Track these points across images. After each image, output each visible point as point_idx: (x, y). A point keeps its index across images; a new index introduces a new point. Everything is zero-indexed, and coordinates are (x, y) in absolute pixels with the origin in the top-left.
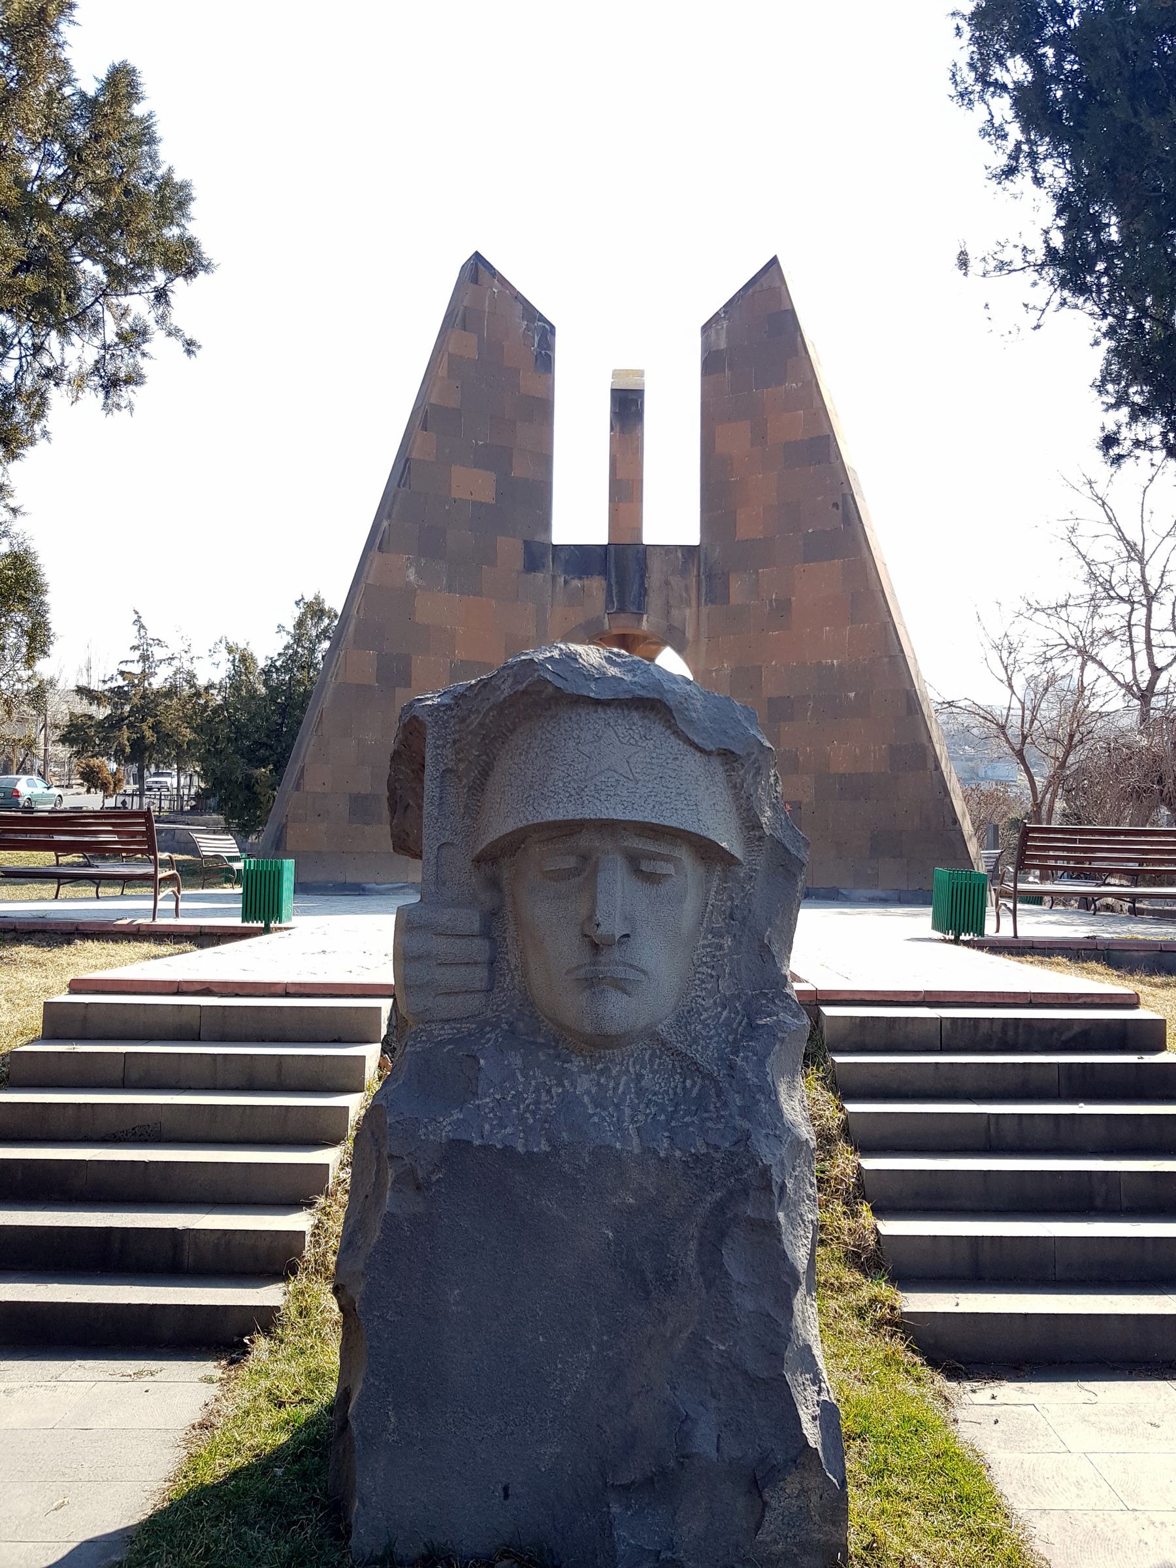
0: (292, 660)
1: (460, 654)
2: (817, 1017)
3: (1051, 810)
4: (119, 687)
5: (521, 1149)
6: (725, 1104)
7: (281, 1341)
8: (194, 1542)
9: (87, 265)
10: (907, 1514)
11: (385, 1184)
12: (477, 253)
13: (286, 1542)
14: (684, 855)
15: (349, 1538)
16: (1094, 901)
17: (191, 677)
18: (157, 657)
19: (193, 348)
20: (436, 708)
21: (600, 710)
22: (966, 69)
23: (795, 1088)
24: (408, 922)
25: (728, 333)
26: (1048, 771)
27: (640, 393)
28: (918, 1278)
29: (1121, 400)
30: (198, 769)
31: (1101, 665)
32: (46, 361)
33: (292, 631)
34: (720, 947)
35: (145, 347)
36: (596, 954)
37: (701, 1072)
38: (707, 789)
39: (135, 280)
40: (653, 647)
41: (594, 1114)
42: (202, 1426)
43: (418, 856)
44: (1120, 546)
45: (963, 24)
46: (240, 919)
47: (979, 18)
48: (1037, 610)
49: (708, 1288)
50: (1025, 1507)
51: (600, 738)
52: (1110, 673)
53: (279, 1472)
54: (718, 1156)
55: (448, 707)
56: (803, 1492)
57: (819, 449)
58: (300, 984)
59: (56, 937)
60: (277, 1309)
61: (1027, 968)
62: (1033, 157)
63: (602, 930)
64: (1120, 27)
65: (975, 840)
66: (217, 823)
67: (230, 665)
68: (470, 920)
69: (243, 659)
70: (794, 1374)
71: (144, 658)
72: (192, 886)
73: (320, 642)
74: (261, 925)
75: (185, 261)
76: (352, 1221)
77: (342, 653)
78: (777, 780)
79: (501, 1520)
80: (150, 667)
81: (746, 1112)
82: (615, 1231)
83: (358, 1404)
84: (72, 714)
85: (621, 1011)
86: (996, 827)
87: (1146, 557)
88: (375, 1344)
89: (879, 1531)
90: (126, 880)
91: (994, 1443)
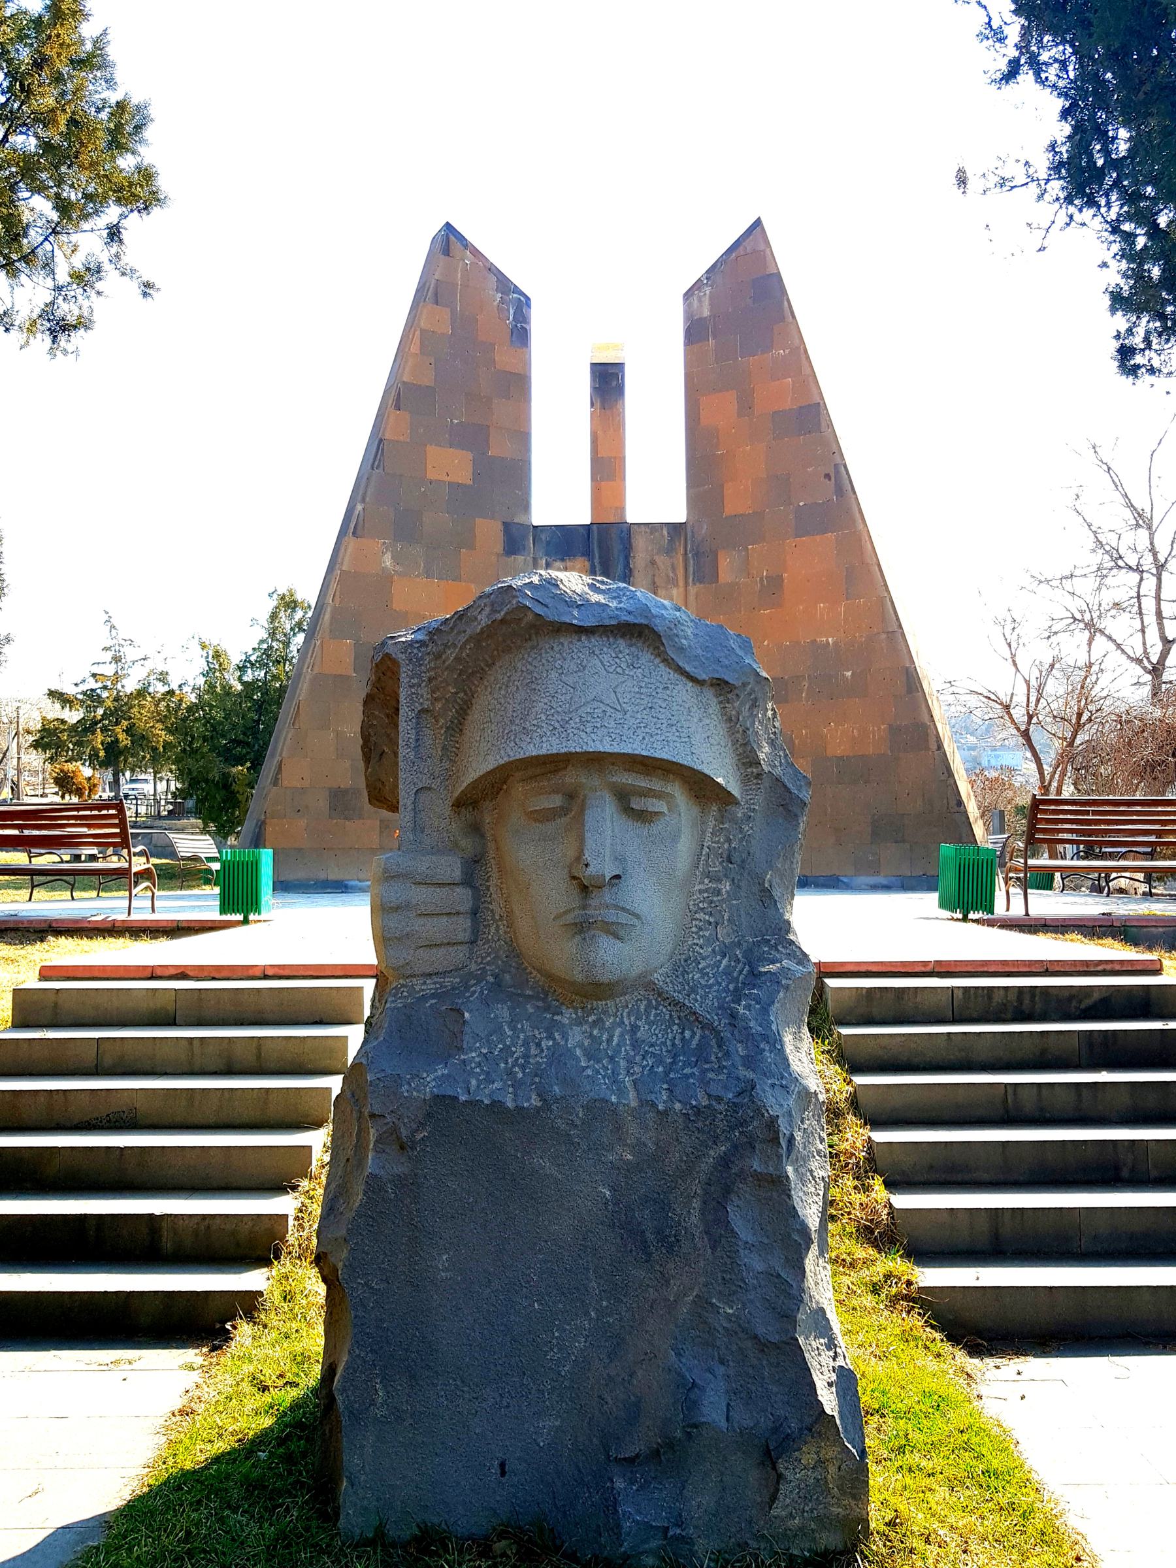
0: (268, 657)
2: (821, 988)
5: (510, 1104)
6: (727, 1054)
7: (265, 1326)
8: (174, 1525)
11: (368, 1146)
13: (271, 1525)
14: (677, 791)
15: (337, 1520)
21: (583, 638)
23: (801, 1039)
28: (935, 1253)
31: (1110, 638)
35: (99, 286)
36: (585, 898)
37: (700, 1022)
38: (700, 720)
42: (182, 1412)
43: (394, 808)
44: (1128, 514)
49: (714, 1248)
52: (1119, 646)
54: (721, 1107)
55: (422, 643)
56: (821, 1463)
57: (809, 418)
59: (27, 934)
60: (261, 1294)
63: (591, 870)
65: (980, 822)
66: (193, 826)
68: (451, 867)
69: (217, 655)
70: (807, 1338)
71: (117, 659)
73: (294, 634)
74: (240, 917)
75: (140, 193)
76: (333, 1186)
77: (318, 643)
78: (775, 714)
79: (498, 1498)
81: (750, 1062)
82: (613, 1189)
83: (343, 1377)
84: (44, 719)
85: (613, 957)
86: (1002, 813)
89: (902, 1507)
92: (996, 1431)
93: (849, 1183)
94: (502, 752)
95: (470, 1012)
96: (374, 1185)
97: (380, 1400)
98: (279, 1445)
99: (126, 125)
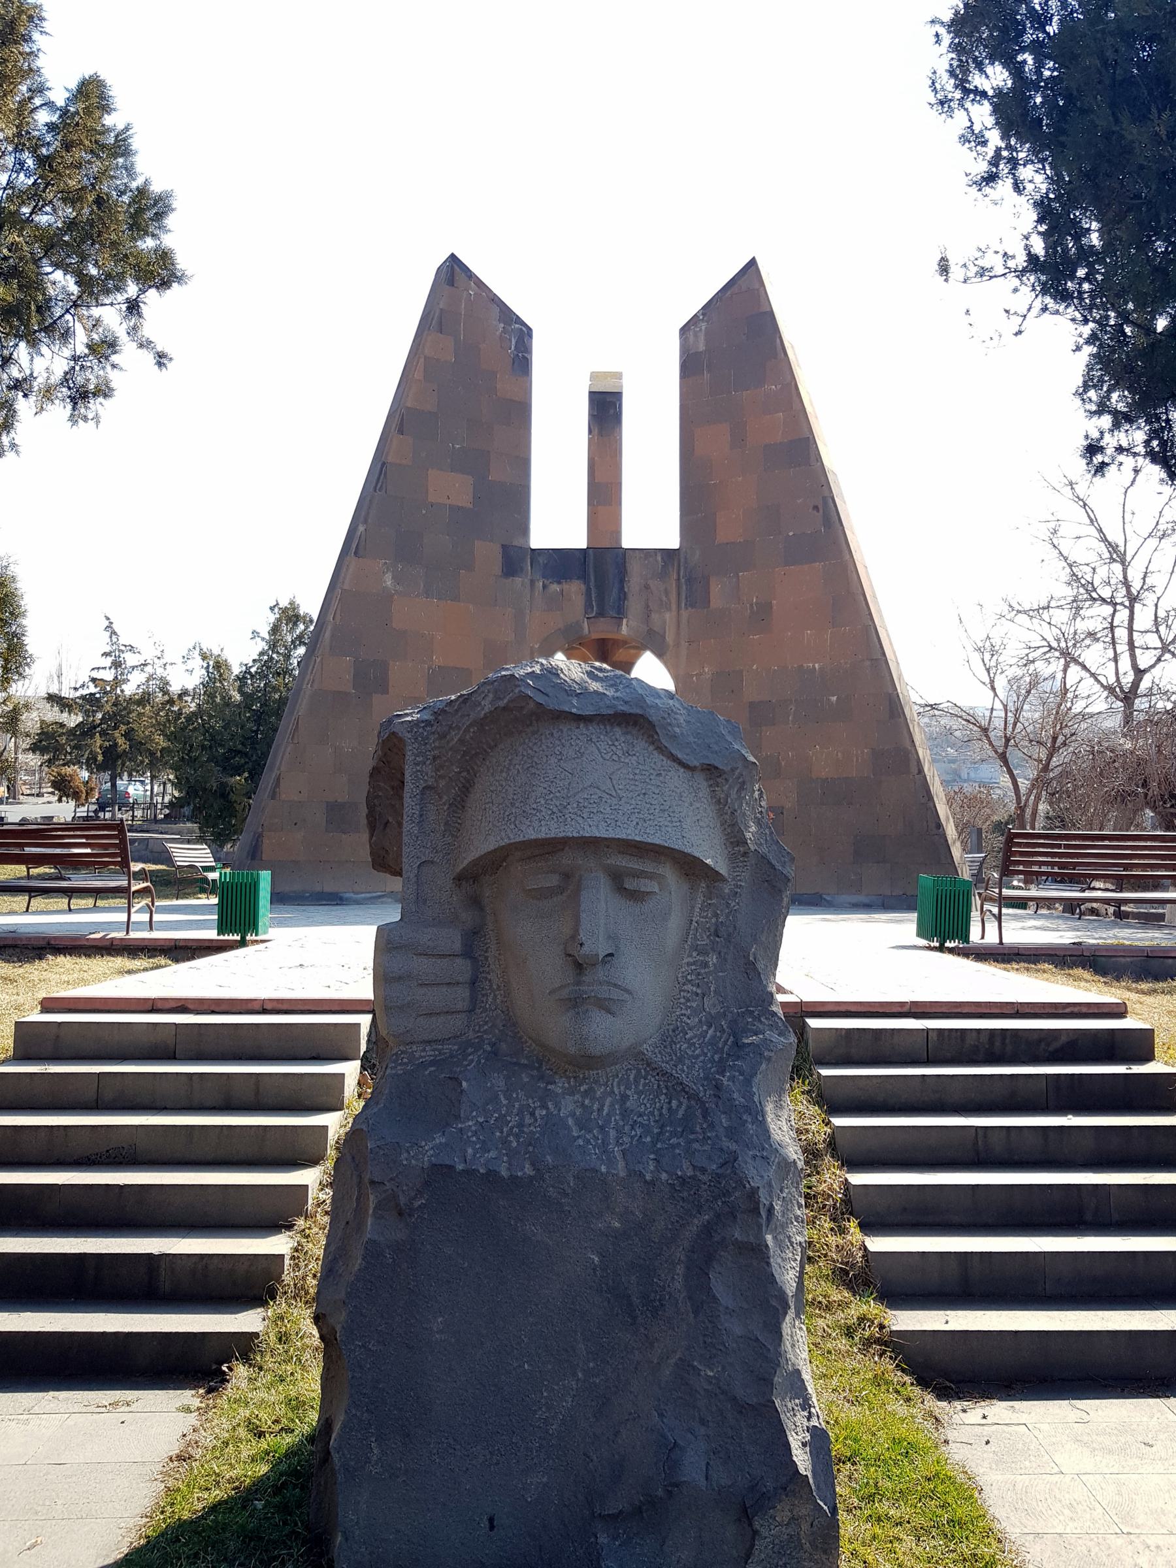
0: (267, 666)
1: (438, 660)
3: (1035, 812)
4: (91, 694)
5: (504, 1173)
6: (712, 1126)
7: (261, 1369)
9: (58, 275)
10: (899, 1540)
11: (367, 1210)
12: (453, 255)
14: (669, 873)
16: (1079, 906)
17: (164, 686)
18: (129, 663)
19: (164, 360)
20: (416, 724)
21: (582, 725)
22: (946, 76)
24: (389, 942)
25: (706, 335)
26: (1032, 773)
27: (618, 395)
29: (1102, 408)
30: (171, 777)
31: (1084, 667)
32: (15, 372)
33: (267, 637)
34: (705, 965)
35: (114, 358)
37: (687, 1093)
39: (108, 292)
40: (632, 651)
41: (578, 1137)
42: (180, 1458)
45: (942, 31)
47: (960, 25)
48: (1019, 612)
50: (1018, 1531)
51: (582, 754)
52: (1093, 675)
53: (259, 1505)
54: (704, 1178)
55: (428, 723)
57: (799, 451)
58: (278, 1001)
59: (27, 951)
60: (256, 1335)
61: (1012, 975)
62: (1014, 163)
63: (586, 949)
64: (1099, 35)
65: (958, 844)
66: (191, 832)
67: (204, 672)
69: (218, 666)
70: (783, 1399)
71: (117, 664)
72: (166, 897)
73: (295, 648)
74: (237, 937)
75: (160, 272)
76: (333, 1248)
77: (318, 660)
78: (761, 795)
80: (122, 674)
81: (733, 1133)
84: (42, 722)
85: (605, 1031)
86: (980, 831)
87: (1128, 558)
88: (358, 1375)
90: (97, 893)
91: (986, 1464)
92: (961, 1478)
93: (826, 1225)
94: (503, 834)
95: (467, 1081)
96: (373, 1252)
97: (375, 1458)
98: (275, 1494)
99: (149, 210)
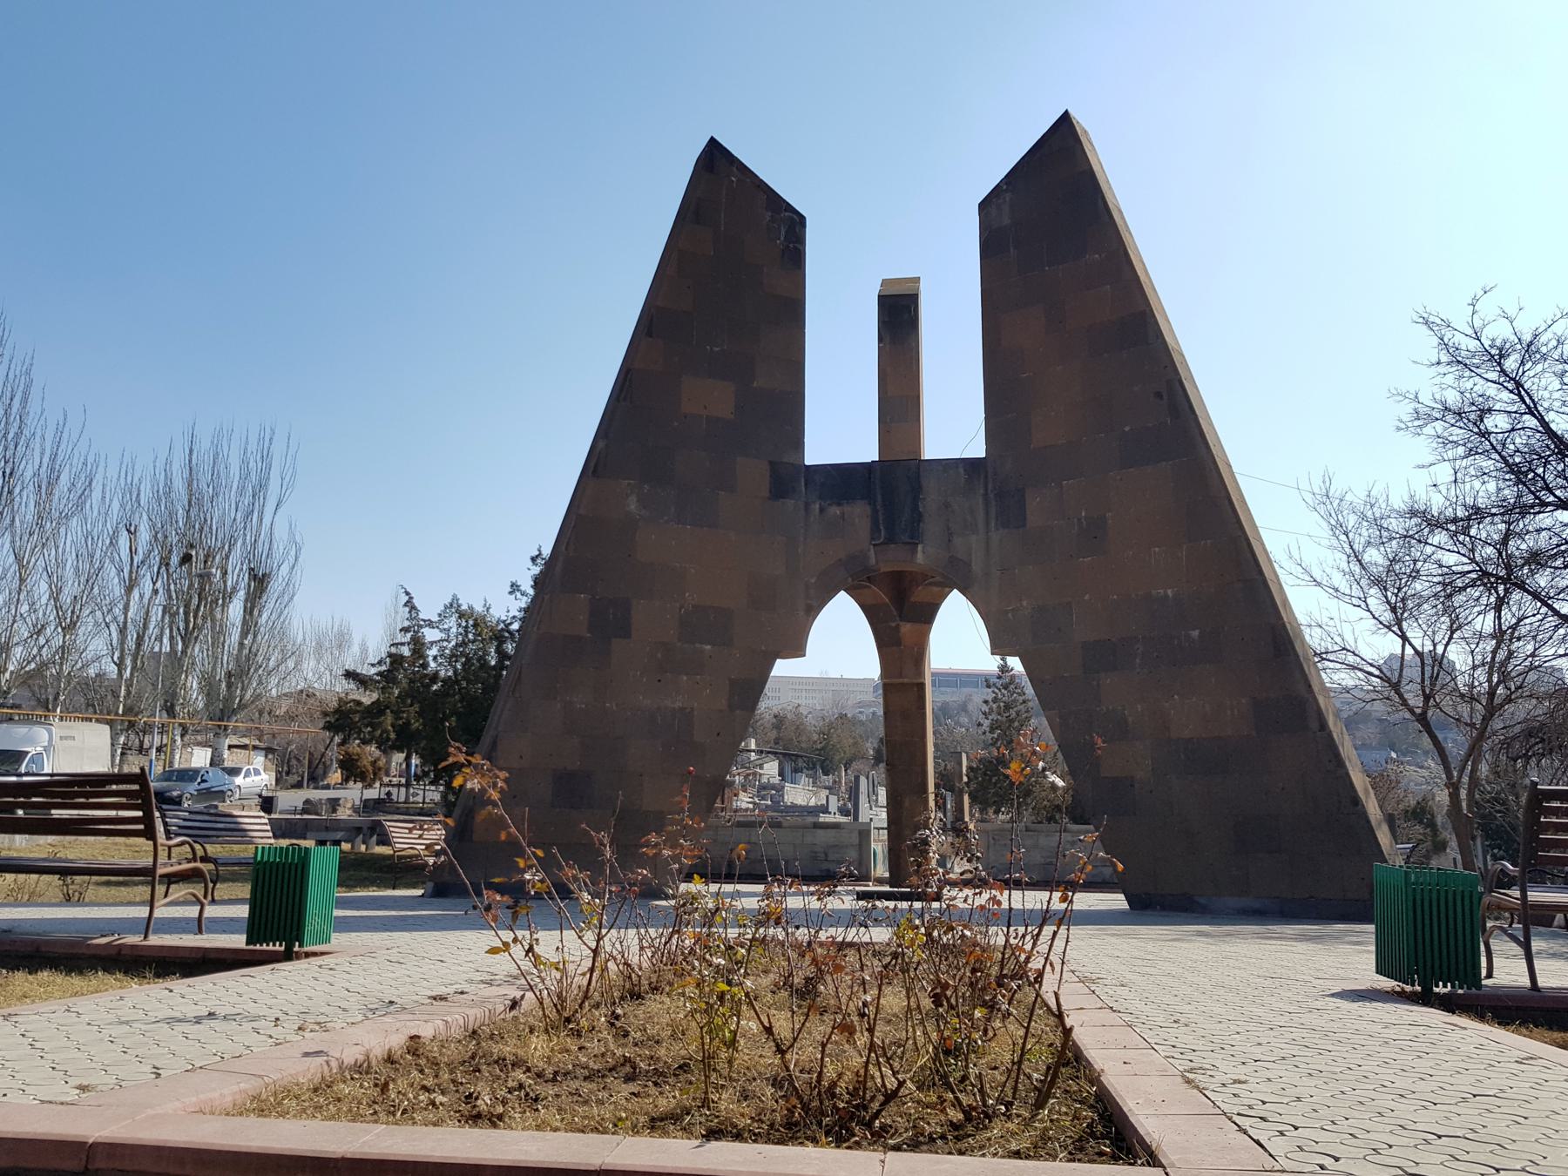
12: (713, 142)
40: (935, 589)
46: (244, 937)
